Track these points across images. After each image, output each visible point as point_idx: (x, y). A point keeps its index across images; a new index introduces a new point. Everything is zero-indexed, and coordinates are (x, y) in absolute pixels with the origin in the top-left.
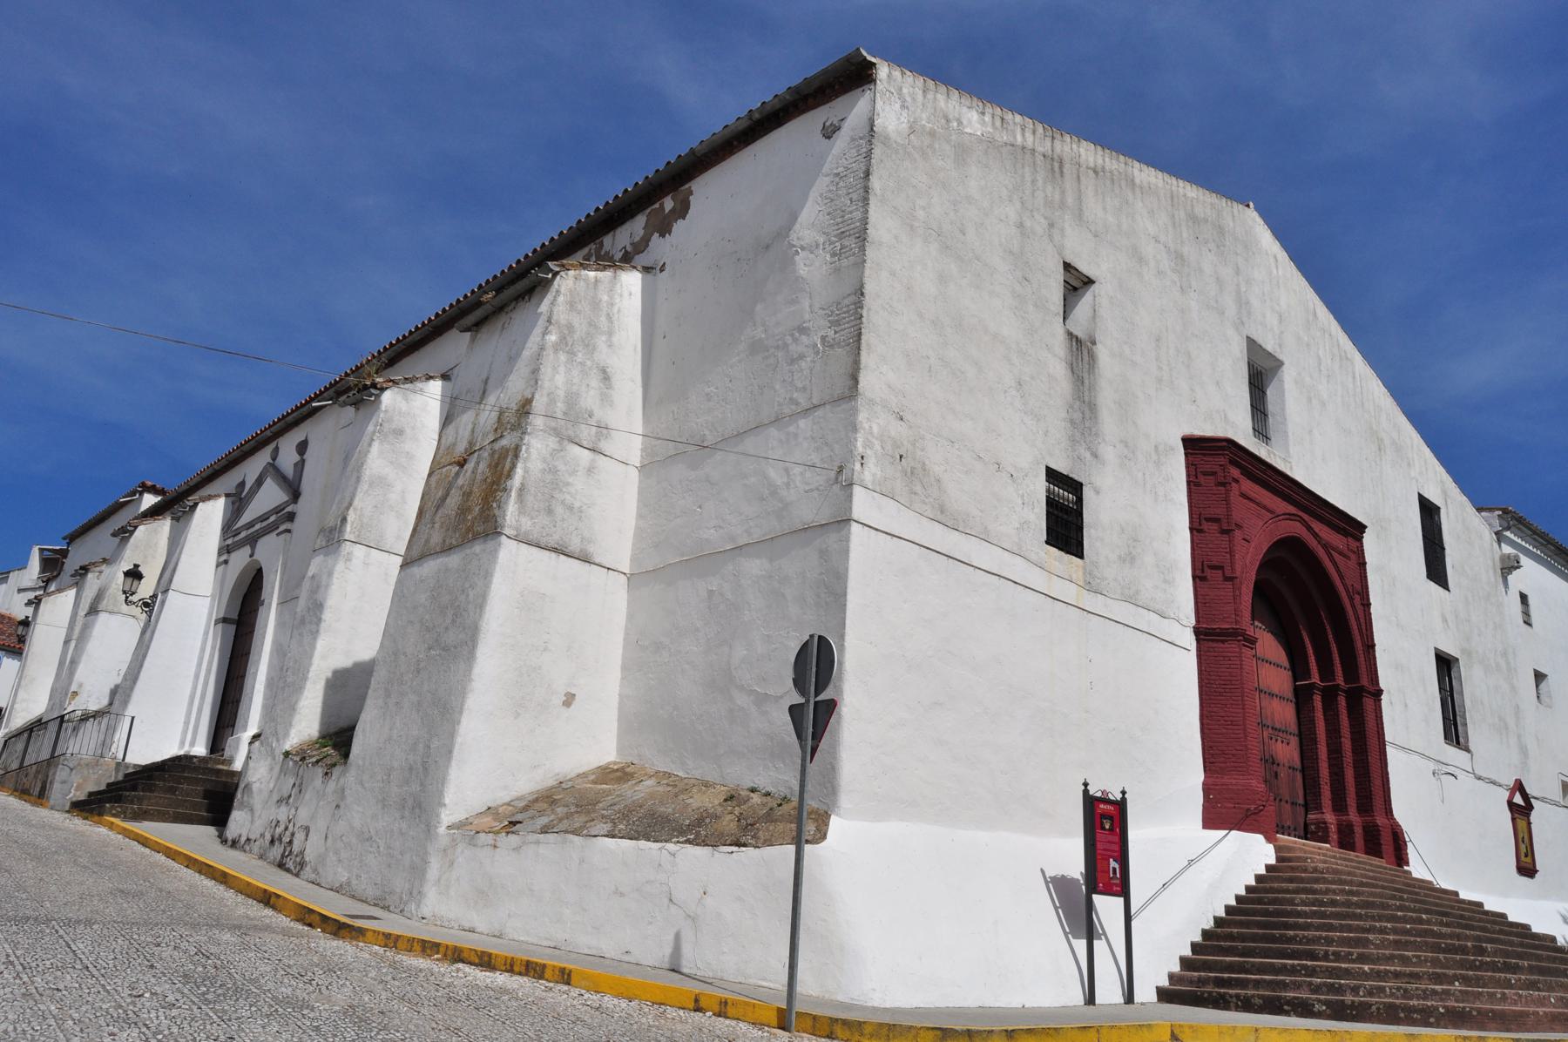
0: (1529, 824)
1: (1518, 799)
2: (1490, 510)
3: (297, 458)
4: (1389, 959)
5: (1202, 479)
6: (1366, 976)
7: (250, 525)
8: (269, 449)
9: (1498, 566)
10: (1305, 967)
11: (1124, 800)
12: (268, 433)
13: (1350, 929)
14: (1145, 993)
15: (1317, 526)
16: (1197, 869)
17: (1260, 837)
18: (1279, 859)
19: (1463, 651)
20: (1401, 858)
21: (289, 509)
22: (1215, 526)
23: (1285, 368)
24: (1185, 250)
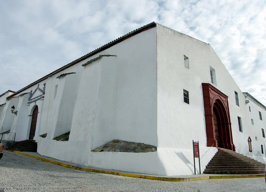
3: (44, 86)
4: (238, 165)
6: (234, 168)
7: (34, 98)
8: (37, 85)
10: (225, 167)
11: (198, 143)
12: (37, 82)
13: (231, 161)
14: (202, 172)
15: (221, 97)
16: (209, 153)
18: (218, 151)
20: (234, 150)
21: (43, 96)
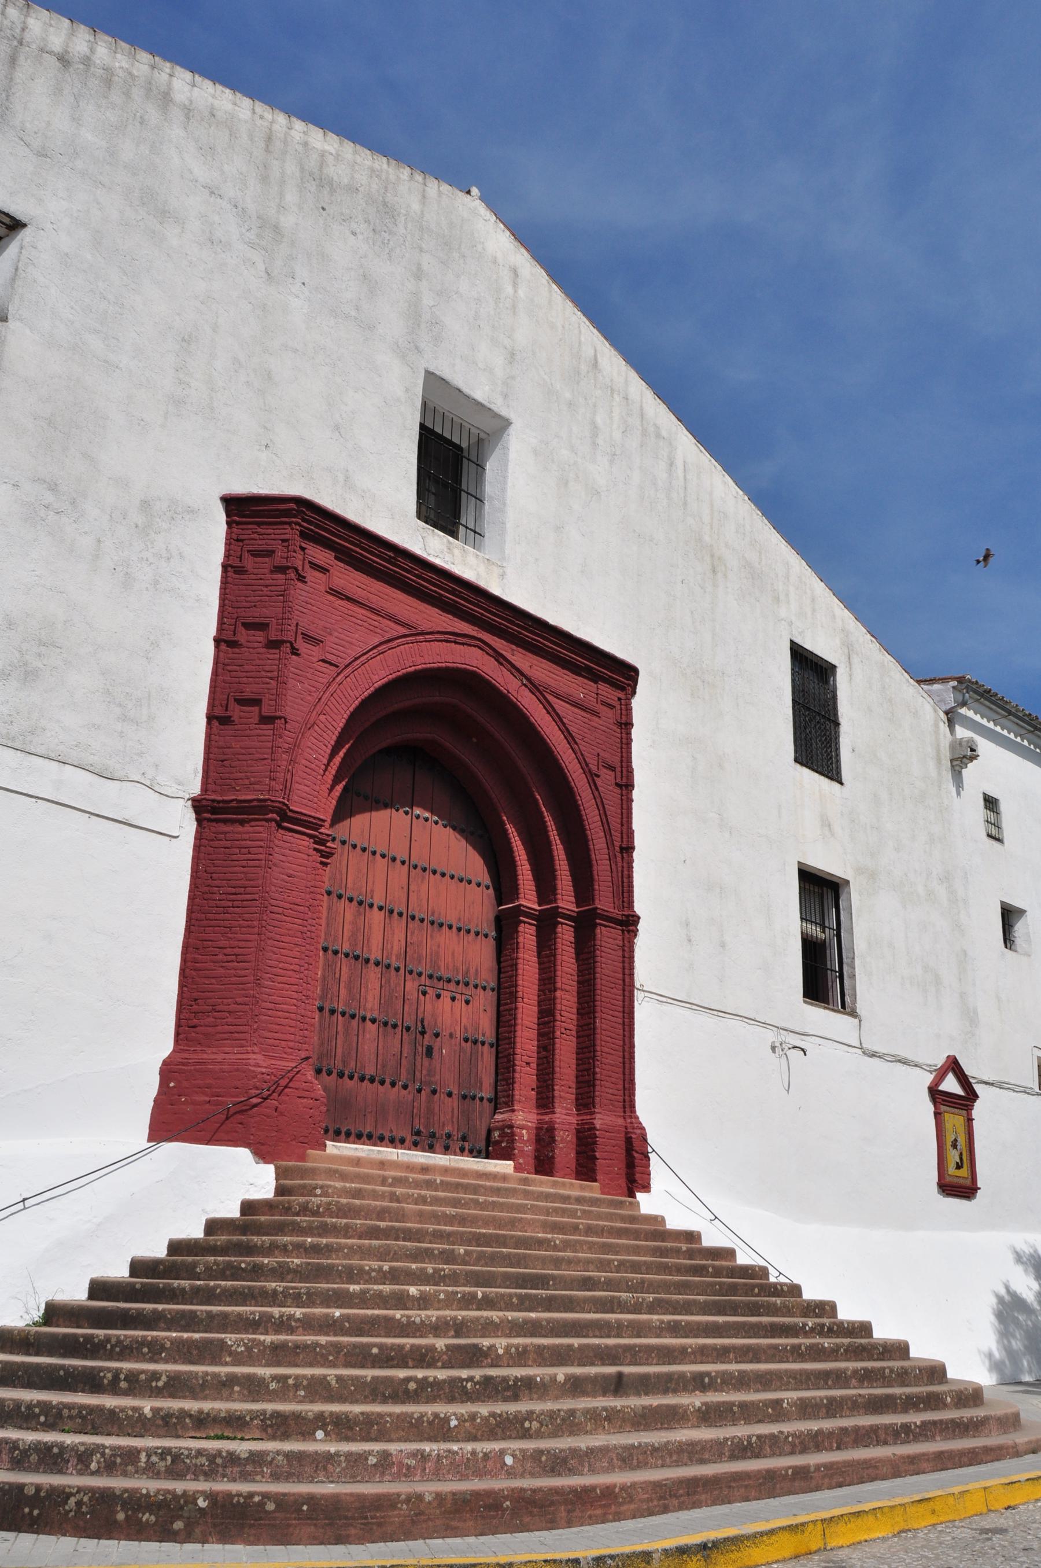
0: (970, 1120)
1: (951, 1085)
2: (944, 680)
5: (249, 562)
9: (946, 755)
17: (244, 1154)
18: (280, 1191)
19: (860, 871)
22: (260, 636)
23: (512, 430)
24: (288, 221)
